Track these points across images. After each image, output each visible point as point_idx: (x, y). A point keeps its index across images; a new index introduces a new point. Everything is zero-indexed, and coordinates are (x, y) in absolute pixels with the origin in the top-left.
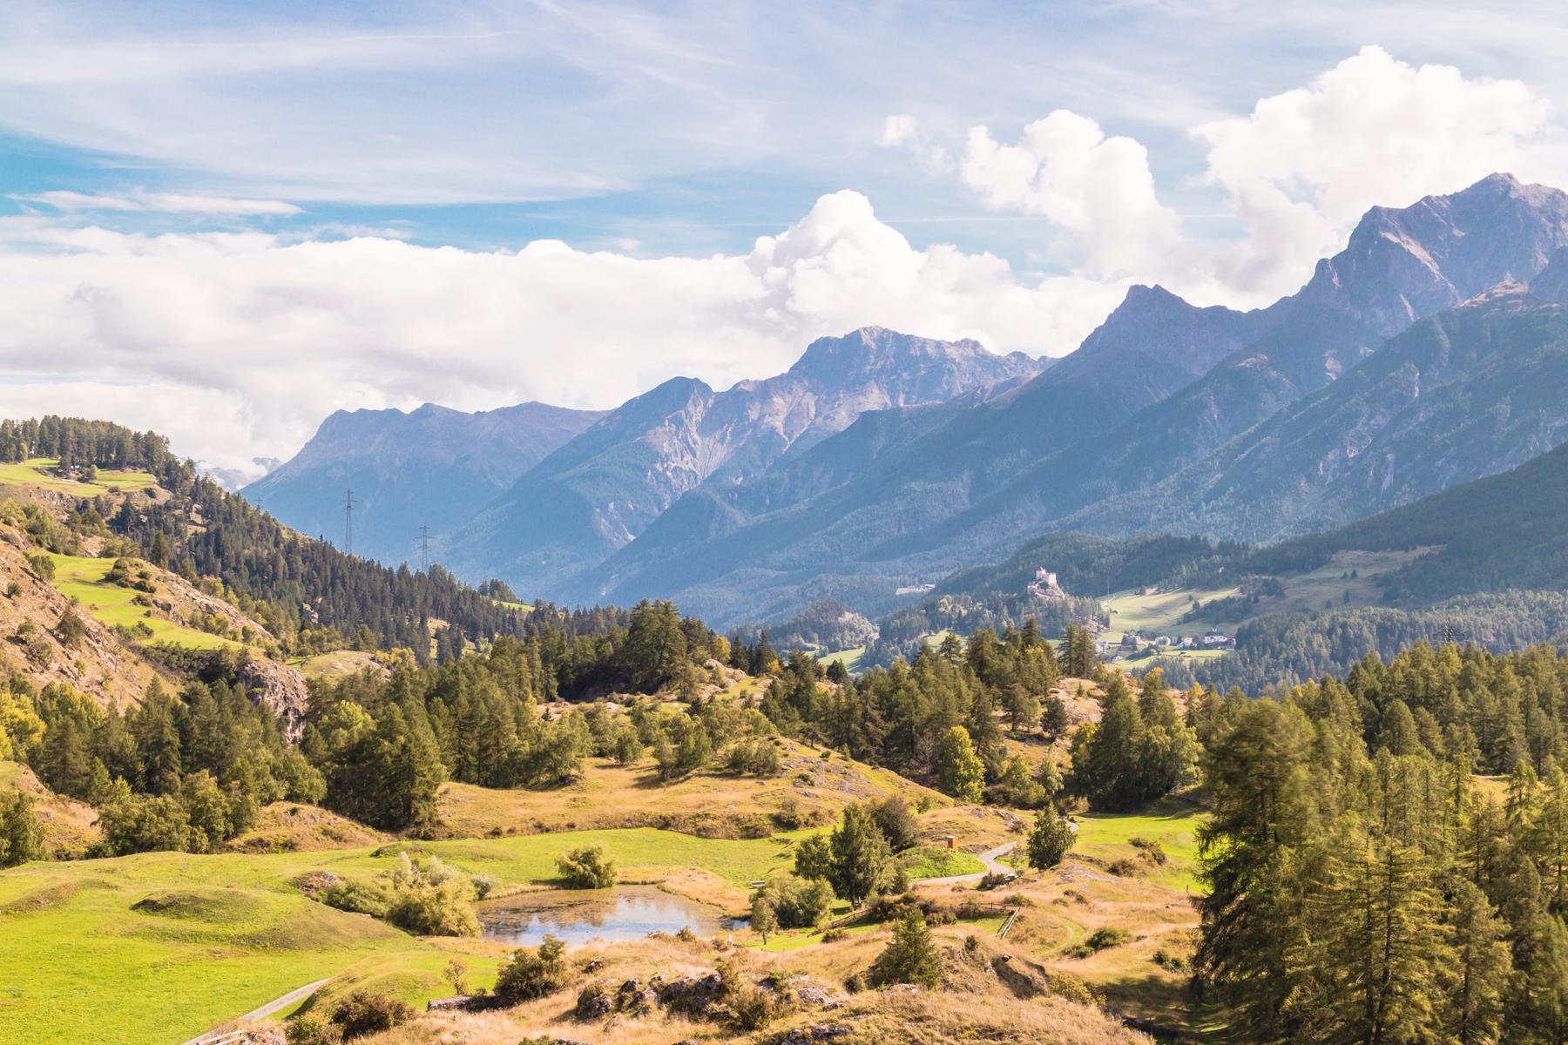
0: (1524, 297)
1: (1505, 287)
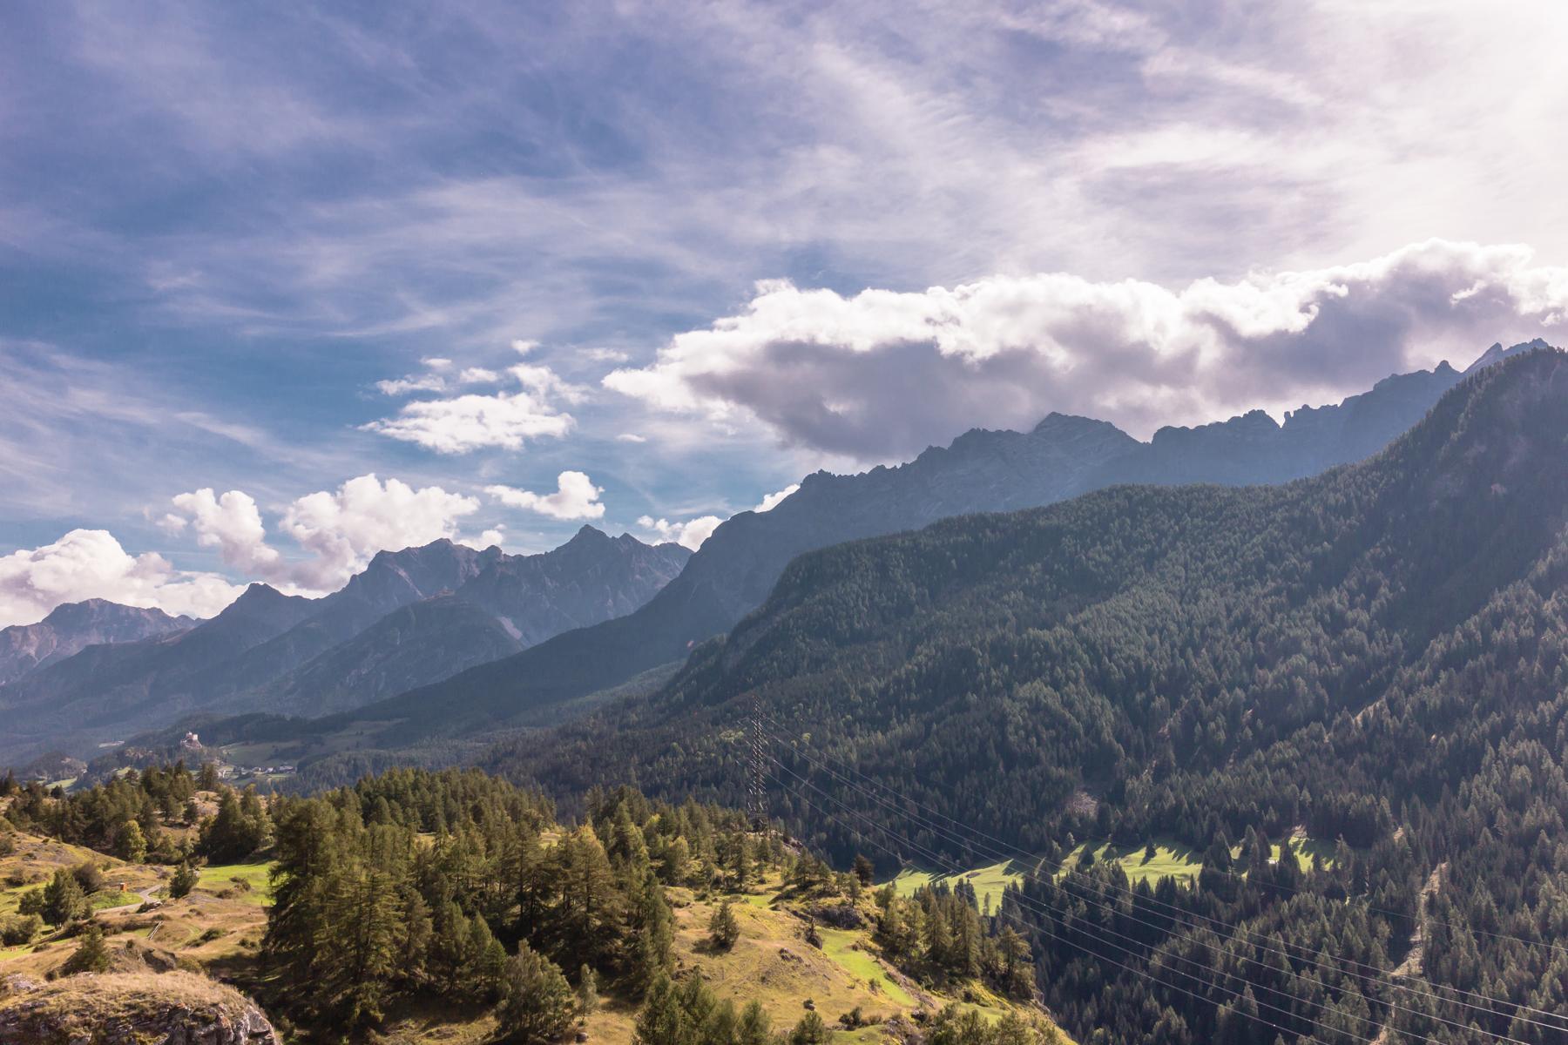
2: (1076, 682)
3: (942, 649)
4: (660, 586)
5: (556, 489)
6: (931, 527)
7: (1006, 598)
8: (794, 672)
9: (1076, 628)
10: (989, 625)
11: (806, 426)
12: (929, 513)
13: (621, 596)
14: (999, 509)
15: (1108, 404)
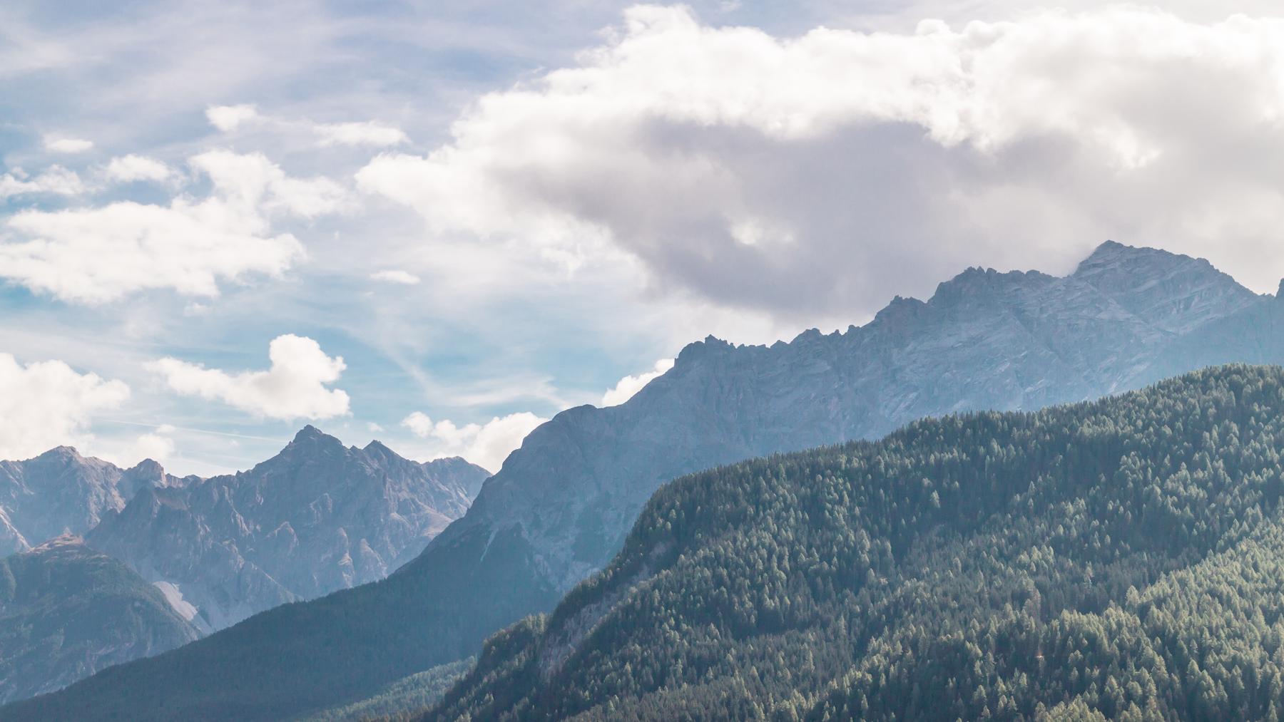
0: (81, 549)
1: (64, 539)
2: (1143, 702)
3: (914, 644)
4: (433, 532)
5: (266, 364)
6: (897, 435)
7: (1024, 557)
8: (661, 680)
9: (1143, 611)
11: (698, 265)
12: (896, 412)
13: (366, 548)
15: (1198, 233)
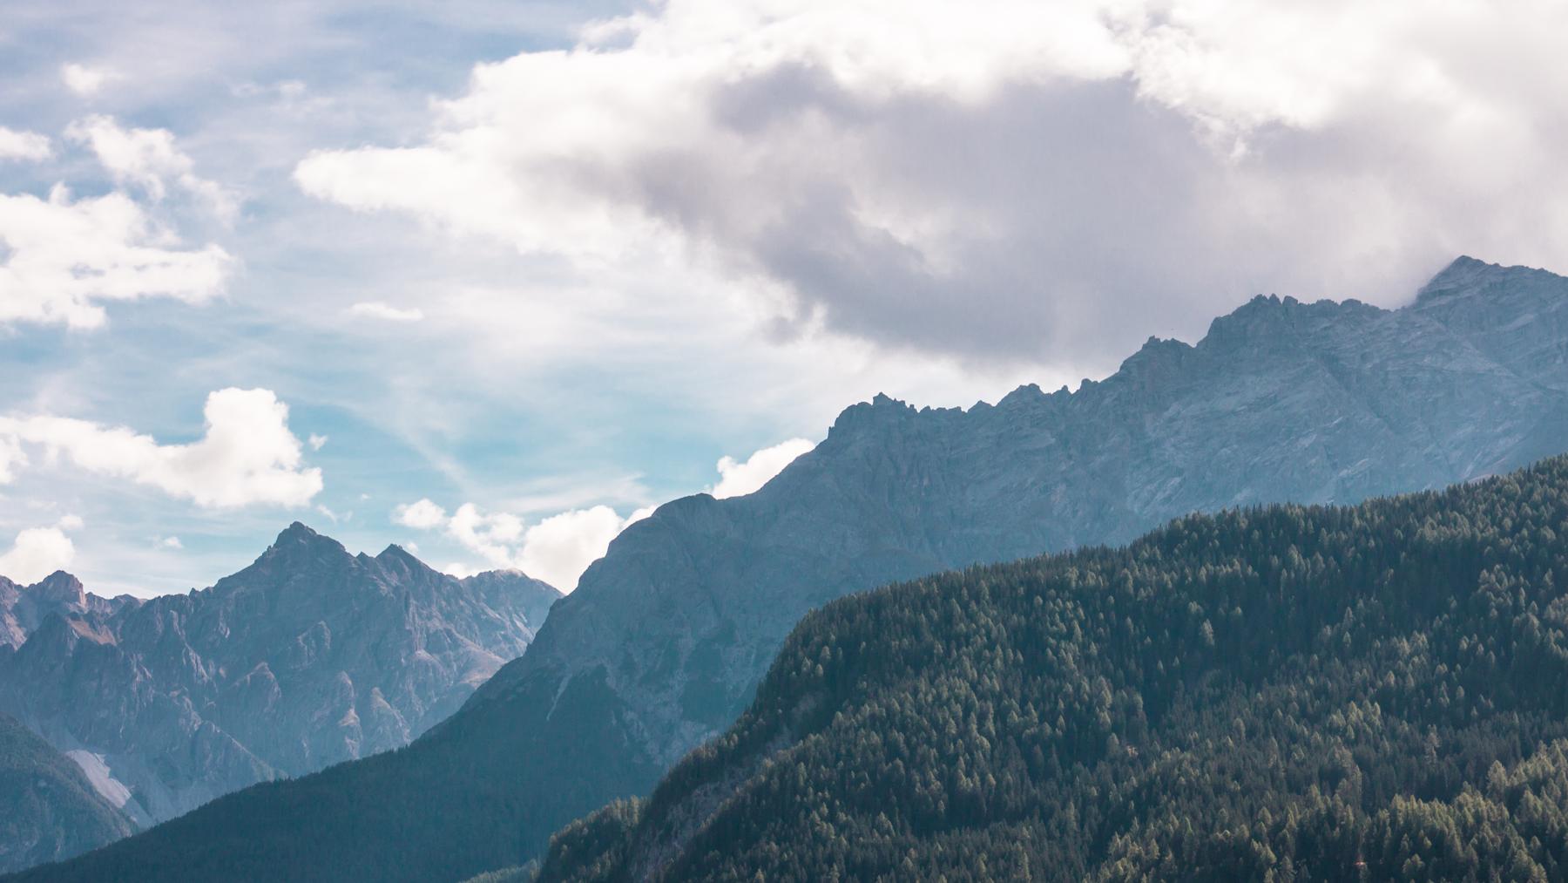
3: (1176, 843)
4: (477, 678)
6: (1153, 539)
7: (1337, 718)
9: (1513, 799)
10: (1296, 787)
12: (1146, 505)
13: (380, 700)
14: (1323, 498)
